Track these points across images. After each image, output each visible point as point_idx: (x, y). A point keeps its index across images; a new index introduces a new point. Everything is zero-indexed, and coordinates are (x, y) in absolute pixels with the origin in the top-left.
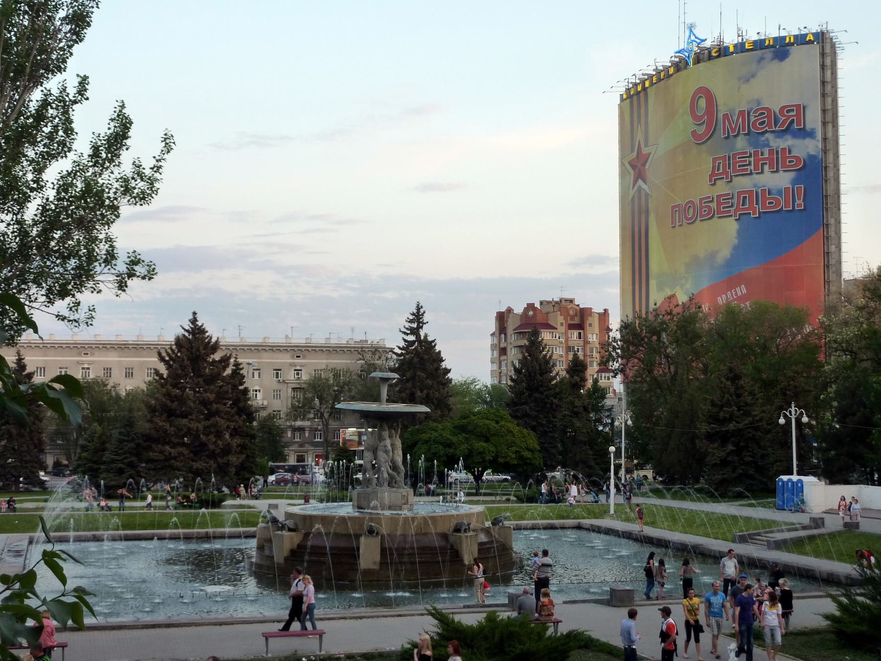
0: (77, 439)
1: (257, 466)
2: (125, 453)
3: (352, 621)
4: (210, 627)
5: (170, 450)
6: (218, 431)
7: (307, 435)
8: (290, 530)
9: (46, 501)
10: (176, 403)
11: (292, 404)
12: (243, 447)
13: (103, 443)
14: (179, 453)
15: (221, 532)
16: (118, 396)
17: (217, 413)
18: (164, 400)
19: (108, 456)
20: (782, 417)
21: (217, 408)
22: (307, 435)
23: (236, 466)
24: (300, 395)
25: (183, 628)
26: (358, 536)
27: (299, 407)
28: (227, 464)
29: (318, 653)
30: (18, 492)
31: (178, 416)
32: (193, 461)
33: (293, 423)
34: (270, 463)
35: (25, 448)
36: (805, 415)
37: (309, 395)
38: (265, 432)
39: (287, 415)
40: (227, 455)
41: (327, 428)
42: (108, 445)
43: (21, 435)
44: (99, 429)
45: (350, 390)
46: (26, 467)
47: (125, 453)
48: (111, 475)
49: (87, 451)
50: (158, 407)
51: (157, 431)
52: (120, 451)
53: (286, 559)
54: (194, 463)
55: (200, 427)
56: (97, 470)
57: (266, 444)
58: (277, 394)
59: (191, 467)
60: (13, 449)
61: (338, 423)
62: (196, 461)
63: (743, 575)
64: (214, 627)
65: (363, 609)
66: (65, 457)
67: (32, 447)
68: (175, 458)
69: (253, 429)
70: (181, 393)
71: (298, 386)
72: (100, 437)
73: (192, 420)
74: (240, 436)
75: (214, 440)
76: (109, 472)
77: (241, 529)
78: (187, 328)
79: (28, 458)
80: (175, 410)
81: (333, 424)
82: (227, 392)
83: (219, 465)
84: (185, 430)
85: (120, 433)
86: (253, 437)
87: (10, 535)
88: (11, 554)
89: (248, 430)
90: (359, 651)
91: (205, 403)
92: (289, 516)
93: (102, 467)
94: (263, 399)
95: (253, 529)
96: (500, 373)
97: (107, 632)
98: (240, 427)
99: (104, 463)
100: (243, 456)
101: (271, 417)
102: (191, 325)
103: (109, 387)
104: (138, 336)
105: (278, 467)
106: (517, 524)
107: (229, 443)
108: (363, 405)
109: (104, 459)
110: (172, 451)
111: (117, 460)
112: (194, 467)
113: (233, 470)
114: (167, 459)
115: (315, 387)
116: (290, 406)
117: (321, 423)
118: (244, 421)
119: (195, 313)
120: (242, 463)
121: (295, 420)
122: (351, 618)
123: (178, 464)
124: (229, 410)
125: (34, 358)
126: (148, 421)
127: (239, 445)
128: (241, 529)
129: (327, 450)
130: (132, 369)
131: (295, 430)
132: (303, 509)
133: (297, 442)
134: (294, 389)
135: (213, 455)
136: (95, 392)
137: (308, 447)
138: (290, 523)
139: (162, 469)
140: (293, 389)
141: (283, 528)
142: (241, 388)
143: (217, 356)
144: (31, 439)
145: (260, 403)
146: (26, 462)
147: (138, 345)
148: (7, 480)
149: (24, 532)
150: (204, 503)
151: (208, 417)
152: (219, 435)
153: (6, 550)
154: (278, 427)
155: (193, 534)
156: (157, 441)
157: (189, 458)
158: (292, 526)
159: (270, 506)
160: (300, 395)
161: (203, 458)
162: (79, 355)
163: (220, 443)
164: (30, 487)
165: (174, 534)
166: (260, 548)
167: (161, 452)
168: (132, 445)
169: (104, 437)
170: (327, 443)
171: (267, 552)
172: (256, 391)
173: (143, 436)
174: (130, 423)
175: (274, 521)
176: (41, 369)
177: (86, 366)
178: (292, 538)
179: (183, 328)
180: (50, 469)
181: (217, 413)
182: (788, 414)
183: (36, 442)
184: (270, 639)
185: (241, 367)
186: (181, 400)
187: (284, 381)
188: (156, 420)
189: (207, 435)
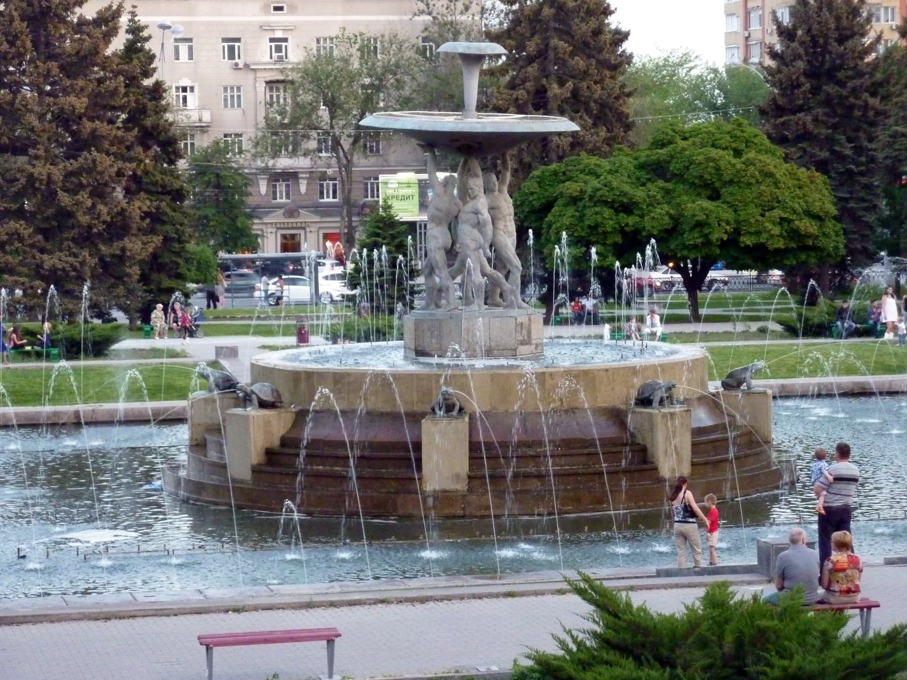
1: (187, 260)
3: (402, 607)
7: (303, 188)
8: (263, 405)
12: (155, 218)
14: (10, 235)
17: (94, 140)
21: (94, 131)
22: (303, 188)
23: (141, 262)
24: (285, 97)
25: (24, 627)
26: (415, 418)
28: (121, 258)
32: (42, 251)
34: (222, 254)
37: (306, 98)
38: (208, 184)
40: (120, 237)
41: (349, 172)
45: (399, 85)
53: (256, 471)
54: (45, 257)
55: (57, 173)
57: (210, 212)
58: (232, 95)
59: (40, 266)
61: (372, 160)
62: (50, 253)
64: (92, 624)
70: (9, 97)
71: (280, 77)
73: (37, 157)
74: (148, 192)
75: (89, 203)
81: (362, 163)
82: (114, 93)
84: (23, 181)
86: (178, 195)
91: (64, 119)
92: (261, 373)
94: (202, 108)
96: (747, 38)
98: (146, 172)
100: (157, 240)
101: (219, 150)
105: (239, 263)
106: (783, 386)
108: (424, 118)
112: (47, 266)
115: (319, 79)
116: (262, 124)
117: (334, 161)
118: (156, 158)
120: (155, 256)
121: (275, 155)
127: (147, 214)
129: (350, 221)
131: (275, 177)
133: (279, 207)
135: (87, 238)
137: (305, 216)
138: (263, 390)
140: (267, 83)
141: (246, 400)
142: (148, 82)
152: (100, 193)
157: (32, 246)
158: (267, 397)
159: (219, 350)
160: (285, 97)
163: (102, 208)
166: (198, 446)
170: (349, 207)
171: (213, 455)
172: (184, 89)
175: (228, 385)
178: (267, 423)
181: (94, 140)
184: (216, 650)
187: (246, 66)
189: (73, 192)
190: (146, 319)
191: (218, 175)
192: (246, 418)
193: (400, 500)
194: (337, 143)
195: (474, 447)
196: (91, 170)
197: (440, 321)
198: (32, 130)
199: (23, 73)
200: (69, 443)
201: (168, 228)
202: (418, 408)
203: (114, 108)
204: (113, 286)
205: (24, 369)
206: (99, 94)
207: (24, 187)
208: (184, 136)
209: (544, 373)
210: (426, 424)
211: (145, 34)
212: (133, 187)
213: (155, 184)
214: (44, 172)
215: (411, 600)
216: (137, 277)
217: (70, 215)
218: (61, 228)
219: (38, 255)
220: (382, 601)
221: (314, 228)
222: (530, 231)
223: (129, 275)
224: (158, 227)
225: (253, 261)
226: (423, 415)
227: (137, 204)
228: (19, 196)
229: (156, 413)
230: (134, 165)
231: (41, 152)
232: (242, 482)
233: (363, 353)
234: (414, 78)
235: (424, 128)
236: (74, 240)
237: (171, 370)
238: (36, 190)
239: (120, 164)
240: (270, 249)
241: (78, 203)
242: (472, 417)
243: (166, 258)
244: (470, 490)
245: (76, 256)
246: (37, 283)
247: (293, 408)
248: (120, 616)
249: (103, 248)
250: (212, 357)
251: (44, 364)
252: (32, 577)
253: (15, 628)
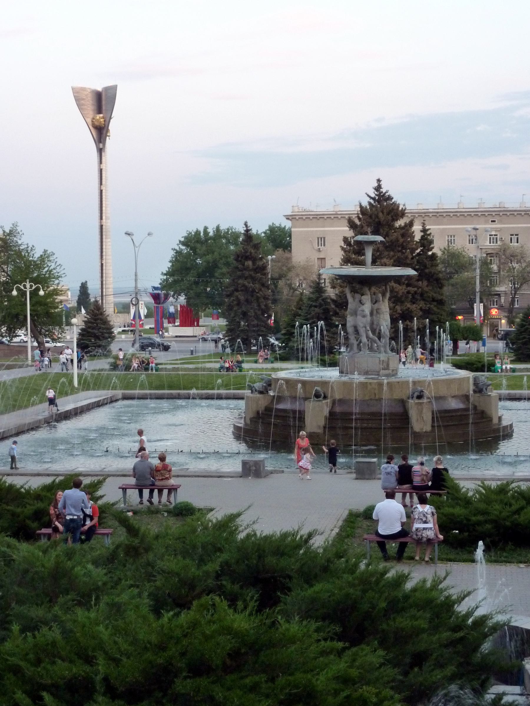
20: (15, 290)
36: (41, 290)
47: (312, 318)
77: (166, 392)
78: (373, 195)
102: (376, 193)
104: (438, 204)
106: (509, 393)
119: (379, 181)
125: (332, 229)
128: (166, 392)
130: (454, 236)
143: (400, 223)
144: (259, 306)
147: (438, 213)
162: (486, 222)
176: (321, 238)
177: (493, 233)
179: (368, 196)
182: (22, 287)
183: (263, 307)
184: (127, 490)
185: (428, 232)
209: (367, 383)
211: (428, 232)
222: (415, 318)
229: (198, 395)
230: (416, 289)
235: (340, 274)
252: (471, 461)
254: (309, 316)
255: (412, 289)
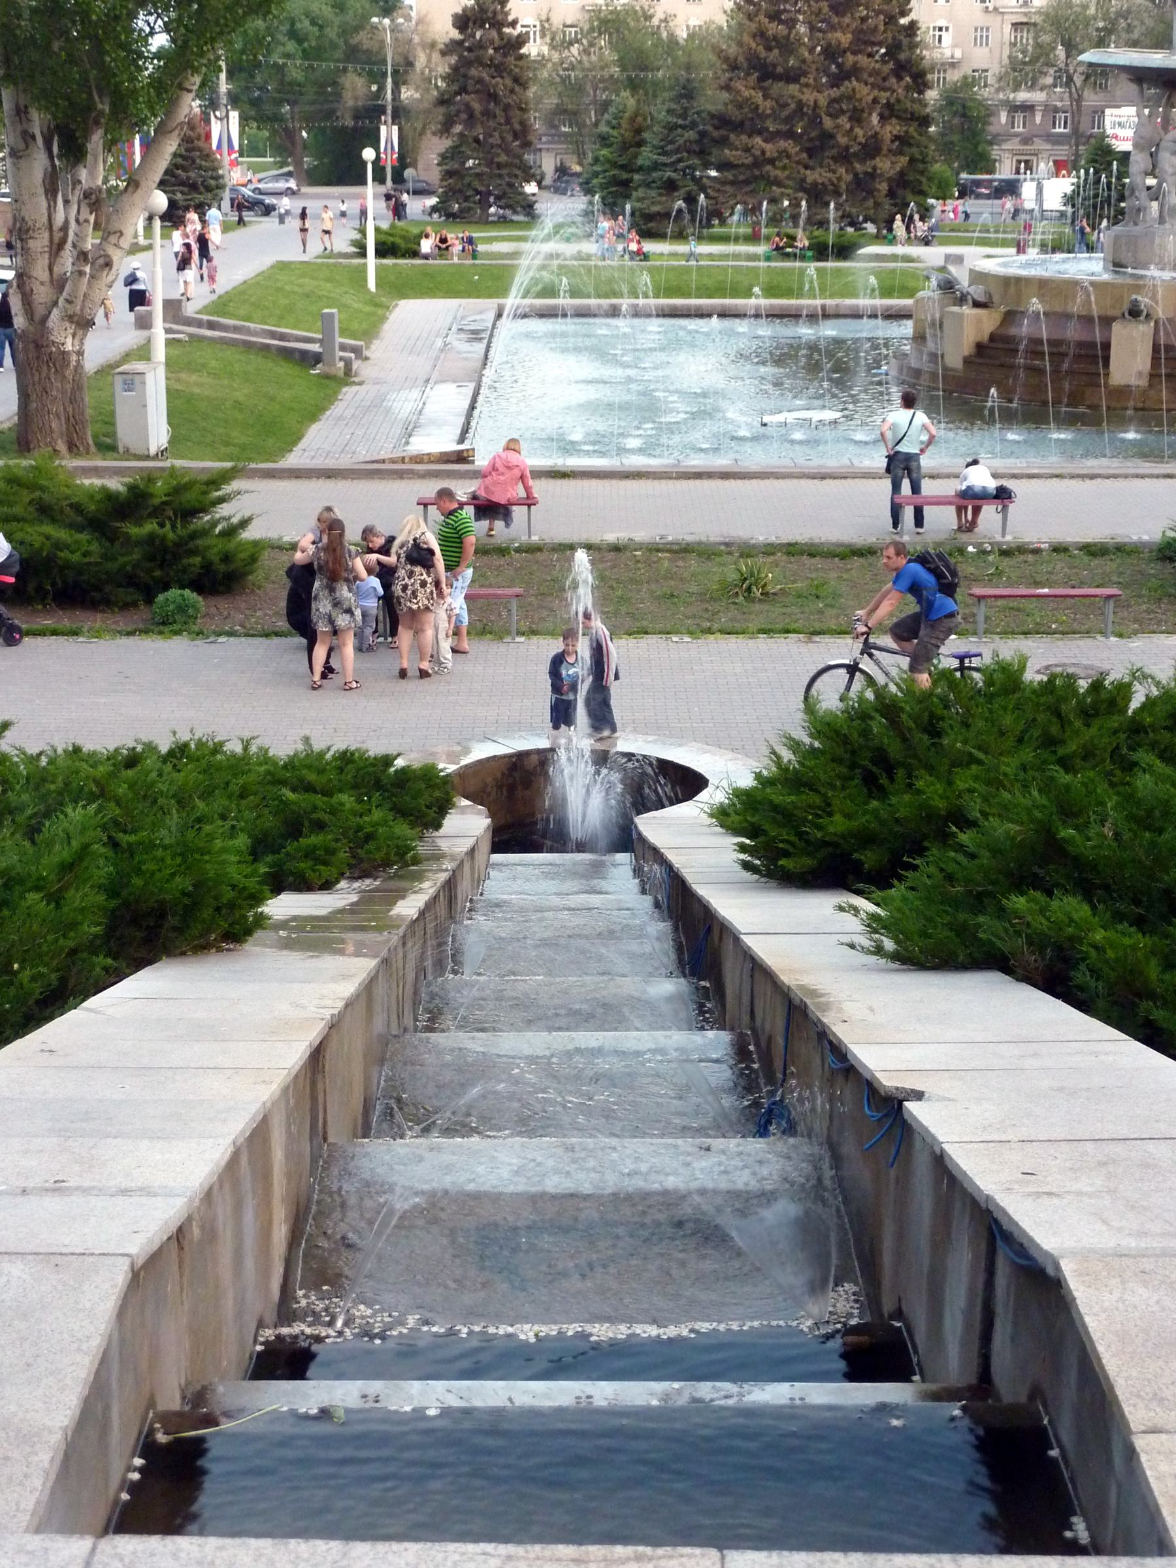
0: (596, 124)
1: (930, 179)
2: (677, 151)
3: (1073, 482)
4: (803, 482)
5: (764, 145)
6: (855, 109)
7: (1038, 119)
8: (977, 304)
9: (524, 239)
10: (776, 51)
11: (1010, 57)
12: (903, 140)
13: (638, 131)
14: (780, 153)
15: (851, 307)
16: (673, 39)
17: (855, 72)
18: (754, 45)
19: (647, 155)
21: (855, 63)
22: (1038, 119)
23: (889, 180)
24: (1027, 37)
25: (754, 481)
26: (1107, 321)
27: (1025, 63)
28: (872, 175)
29: (999, 538)
30: (485, 222)
31: (778, 78)
32: (806, 167)
33: (1012, 96)
34: (964, 175)
35: (495, 140)
37: (1045, 38)
38: (955, 114)
39: (1000, 79)
40: (873, 157)
41: (1079, 106)
42: (646, 135)
43: (487, 113)
44: (632, 103)
45: (1129, 29)
46: (500, 176)
47: (677, 151)
48: (653, 193)
49: (610, 145)
50: (741, 59)
51: (740, 107)
52: (669, 147)
53: (967, 361)
54: (808, 172)
55: (823, 101)
56: (626, 184)
57: (955, 138)
58: (982, 36)
59: (803, 180)
60: (477, 141)
61: (1101, 95)
62: (812, 169)
63: (986, 412)
64: (810, 482)
65: (1104, 461)
66: (575, 158)
67: (510, 138)
68: (772, 161)
69: (926, 106)
70: (785, 32)
71: (1025, 20)
72: (632, 120)
73: (807, 85)
74: (898, 117)
75: (848, 126)
76: (648, 185)
79: (503, 158)
80: (775, 66)
81: (1091, 98)
82: (875, 30)
83: (856, 175)
84: (793, 106)
85: (669, 111)
86: (925, 121)
87: (463, 301)
88: (462, 336)
89: (915, 106)
90: (1078, 539)
91: (831, 53)
92: (978, 277)
93: (636, 177)
94: (955, 46)
95: (909, 302)
97: (614, 482)
98: (898, 101)
99: (640, 169)
100: (904, 160)
101: (968, 83)
103: (655, 21)
105: (978, 183)
107: (876, 133)
108: (1135, 55)
109: (640, 162)
110: (768, 147)
111: (665, 165)
112: (809, 180)
113: (883, 187)
114: (757, 164)
115: (1059, 22)
116: (1006, 61)
117: (1067, 95)
118: (907, 88)
120: (902, 174)
121: (1016, 89)
122: (1072, 477)
123: (778, 173)
124: (878, 66)
126: (722, 88)
127: (897, 138)
129: (1077, 150)
131: (1016, 109)
132: (1005, 265)
133: (1016, 135)
134: (1016, 26)
135: (844, 157)
136: (629, 30)
137: (1039, 144)
138: (977, 292)
139: (747, 182)
140: (1014, 25)
141: (962, 300)
142: (903, 21)
144: (508, 121)
145: (948, 53)
146: (499, 166)
148: (466, 199)
149: (490, 296)
150: (820, 251)
151: (836, 82)
152: (857, 117)
153: (454, 328)
154: (980, 103)
155: (800, 308)
156: (738, 126)
157: (798, 163)
158: (981, 298)
159: (948, 258)
160: (1027, 37)
161: (826, 161)
163: (859, 131)
164: (508, 212)
165: (583, 306)
166: (919, 338)
167: (747, 150)
168: (691, 135)
169: (640, 119)
170: (1077, 136)
171: (931, 345)
172: (940, 29)
173: (713, 116)
174: (687, 92)
175: (948, 286)
178: (979, 320)
180: (548, 181)
181: (855, 72)
183: (517, 127)
186: (786, 46)
187: (996, 9)
188: (739, 85)
189: (834, 116)
190: (890, 230)
191: (964, 107)
192: (961, 316)
193: (1088, 391)
194: (1070, 79)
195: (1156, 349)
196: (850, 97)
197: (1136, 237)
198: (804, 61)
199: (799, 11)
200: (829, 330)
201: (914, 150)
202: (1111, 313)
203: (873, 44)
204: (864, 199)
205: (782, 269)
206: (862, 31)
207: (795, 112)
208: (932, 69)
210: (1116, 327)
212: (887, 113)
213: (906, 111)
214: (812, 99)
215: (1082, 477)
216: (884, 192)
217: (831, 136)
218: (822, 148)
219: (802, 171)
220: (1057, 476)
221: (1045, 155)
223: (878, 191)
224: (906, 149)
225: (992, 181)
226: (1114, 319)
227: (888, 128)
228: (788, 120)
231: (811, 81)
232: (953, 370)
233: (1064, 261)
234: (1143, 23)
236: (833, 158)
237: (904, 272)
238: (803, 114)
239: (876, 92)
240: (1005, 172)
241: (838, 127)
242: (1156, 322)
243: (911, 177)
244: (1150, 386)
245: (834, 172)
246: (800, 194)
247: (1003, 309)
248: (833, 477)
249: (858, 166)
250: (941, 263)
251: (798, 264)
253: (747, 482)
254: (669, 147)
255: (884, 96)
